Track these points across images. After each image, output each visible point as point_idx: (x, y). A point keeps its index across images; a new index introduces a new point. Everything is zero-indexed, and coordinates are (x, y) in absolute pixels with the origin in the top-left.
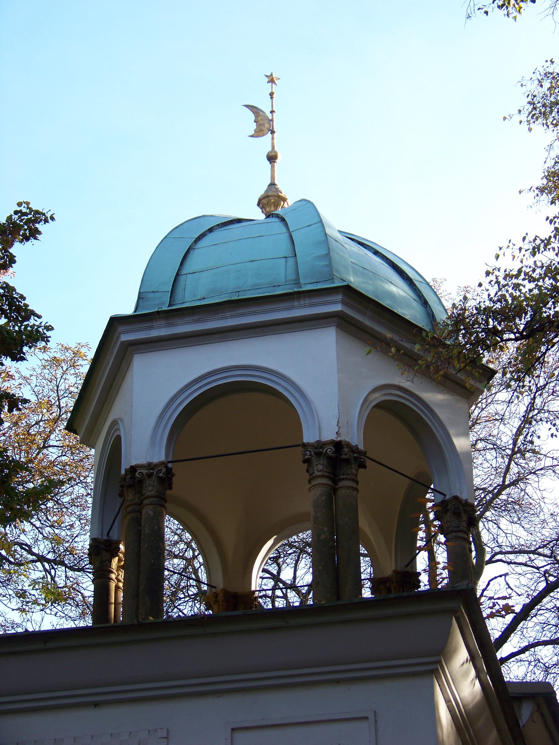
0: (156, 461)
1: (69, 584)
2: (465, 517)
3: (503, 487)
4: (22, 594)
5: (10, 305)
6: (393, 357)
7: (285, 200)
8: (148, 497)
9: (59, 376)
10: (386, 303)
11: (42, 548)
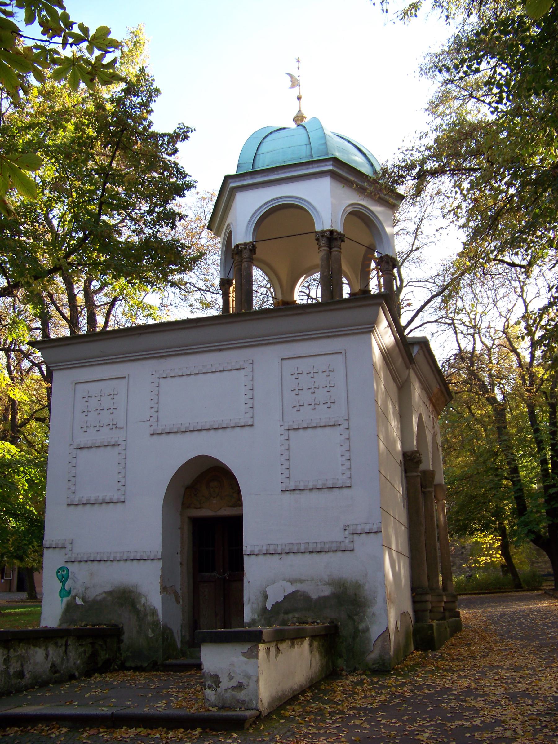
0: (248, 241)
1: (213, 300)
2: (391, 264)
3: (412, 251)
4: (191, 305)
5: (177, 172)
6: (355, 189)
7: (305, 118)
8: (245, 258)
9: (205, 206)
10: (353, 165)
11: (201, 285)
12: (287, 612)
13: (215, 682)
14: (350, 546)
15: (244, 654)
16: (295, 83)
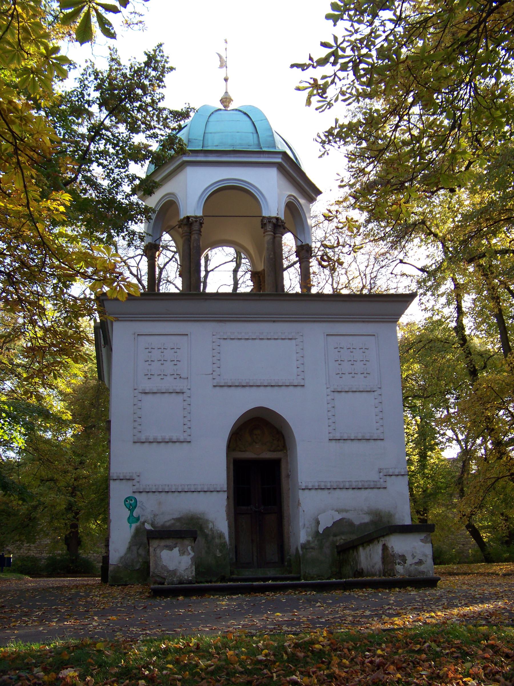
12: (335, 535)
13: (402, 560)
14: (384, 485)
15: (422, 540)
16: (223, 64)
